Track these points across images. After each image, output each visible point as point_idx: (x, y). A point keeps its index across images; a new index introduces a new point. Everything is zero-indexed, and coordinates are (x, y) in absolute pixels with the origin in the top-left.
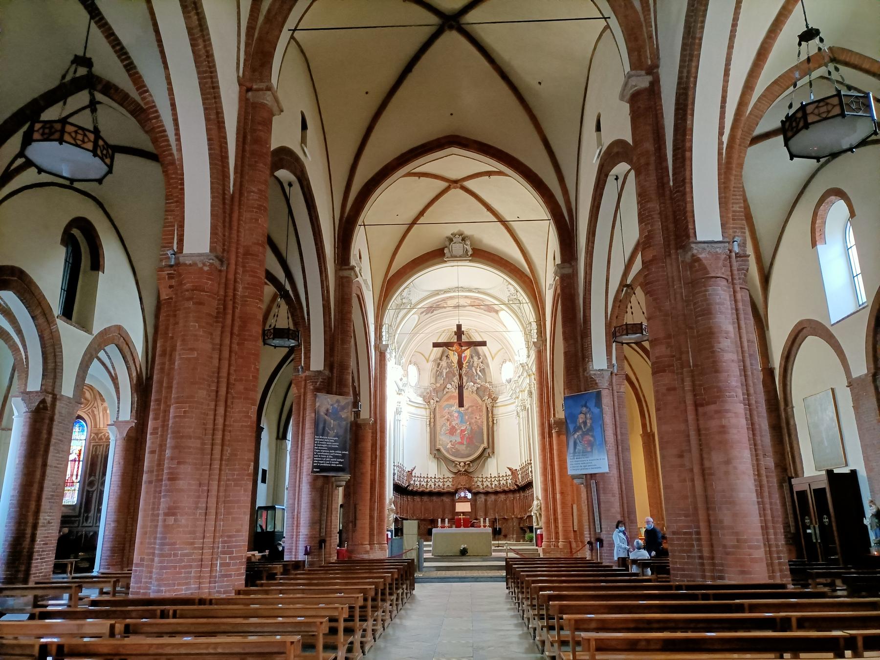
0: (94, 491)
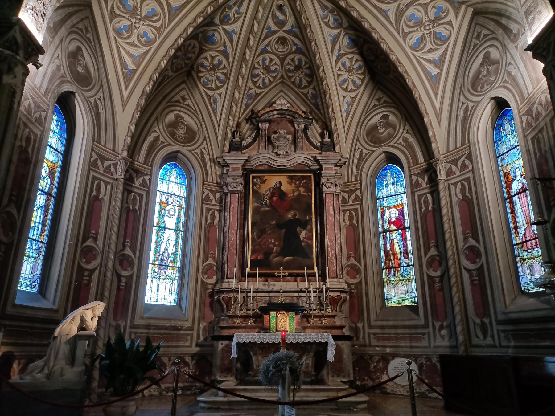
0: (92, 271)
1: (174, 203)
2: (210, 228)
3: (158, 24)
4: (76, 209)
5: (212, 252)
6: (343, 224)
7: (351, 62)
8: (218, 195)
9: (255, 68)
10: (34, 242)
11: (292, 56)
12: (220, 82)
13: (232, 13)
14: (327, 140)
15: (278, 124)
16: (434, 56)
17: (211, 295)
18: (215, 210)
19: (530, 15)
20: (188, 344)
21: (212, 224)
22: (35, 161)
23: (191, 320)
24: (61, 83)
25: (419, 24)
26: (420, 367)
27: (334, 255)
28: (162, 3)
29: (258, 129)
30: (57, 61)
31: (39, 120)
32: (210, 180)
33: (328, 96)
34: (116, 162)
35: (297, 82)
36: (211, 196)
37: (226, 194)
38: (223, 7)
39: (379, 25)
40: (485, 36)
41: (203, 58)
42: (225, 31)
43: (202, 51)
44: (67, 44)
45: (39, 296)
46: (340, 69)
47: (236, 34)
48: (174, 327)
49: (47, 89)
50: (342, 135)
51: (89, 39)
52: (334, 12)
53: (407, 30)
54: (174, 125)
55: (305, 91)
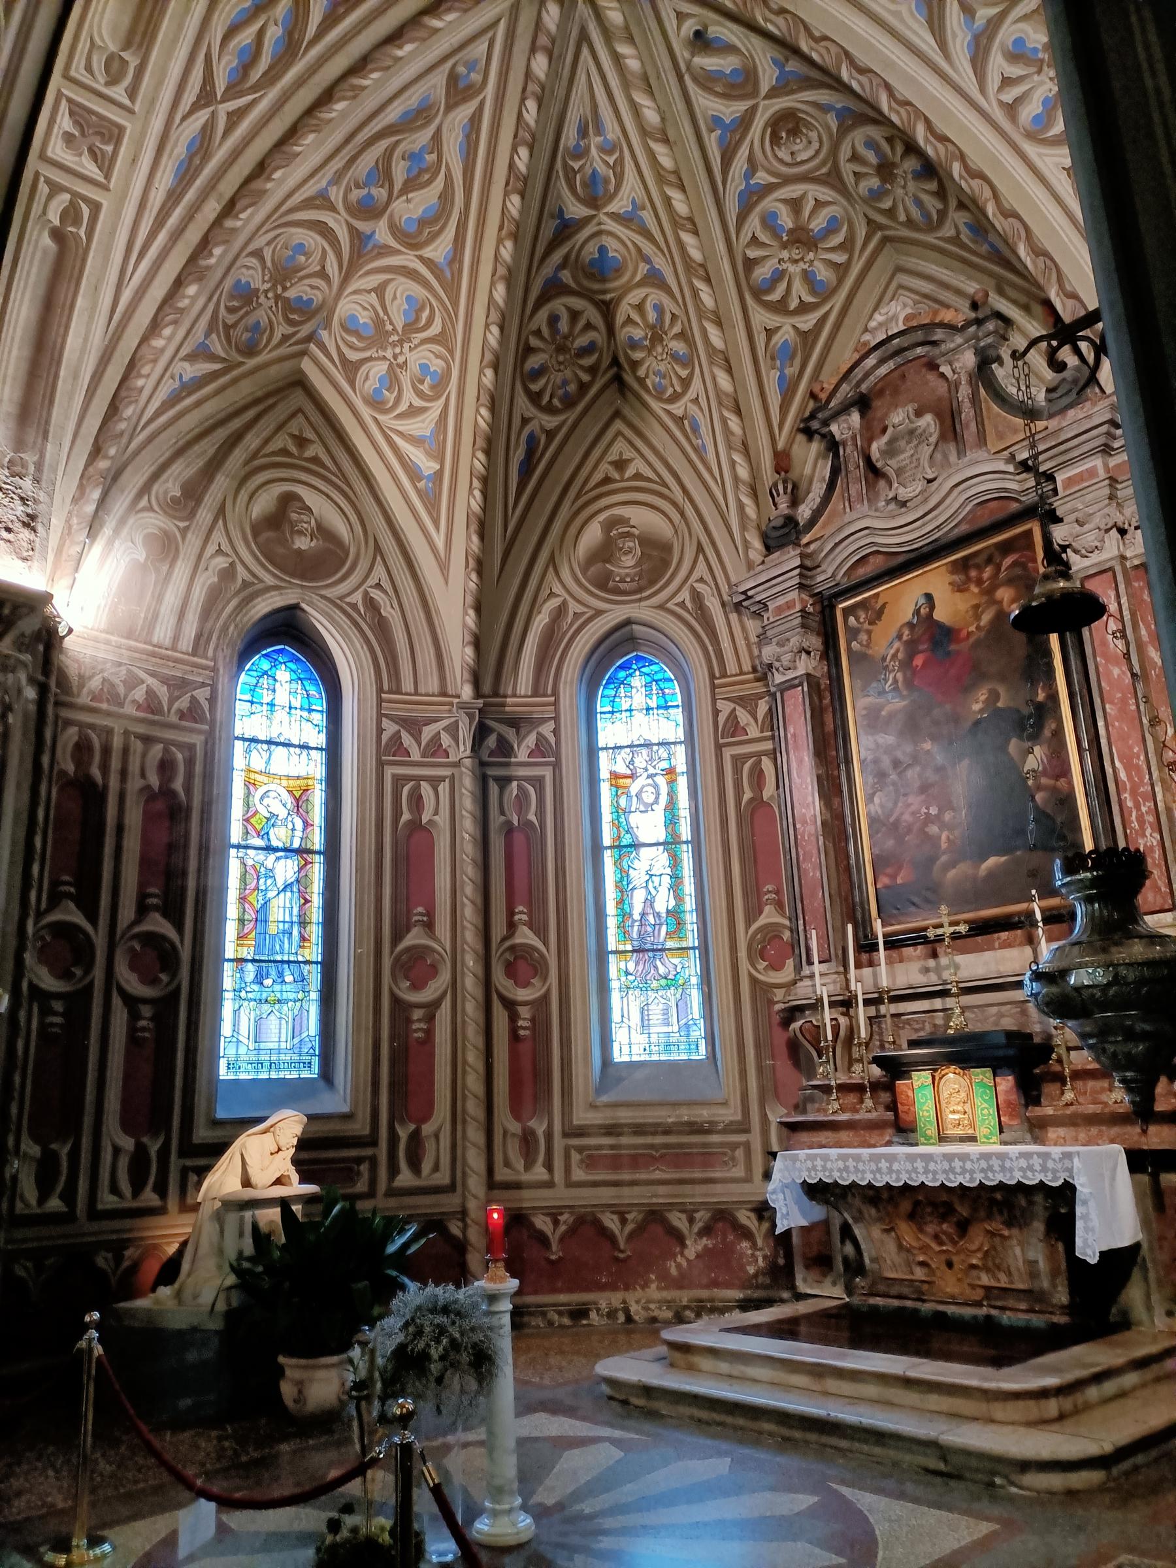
0: (432, 1007)
1: (649, 767)
2: (752, 814)
3: (435, 329)
5: (770, 887)
8: (763, 707)
9: (750, 264)
10: (286, 966)
11: (845, 152)
12: (684, 365)
18: (759, 755)
20: (739, 1172)
22: (203, 802)
23: (735, 1100)
27: (1150, 818)
29: (833, 445)
31: (192, 713)
32: (732, 667)
34: (453, 720)
35: (915, 213)
36: (743, 716)
38: (559, 165)
43: (607, 309)
44: (244, 505)
45: (322, 1084)
47: (643, 208)
48: (690, 1124)
49: (198, 637)
54: (605, 552)
55: (948, 231)
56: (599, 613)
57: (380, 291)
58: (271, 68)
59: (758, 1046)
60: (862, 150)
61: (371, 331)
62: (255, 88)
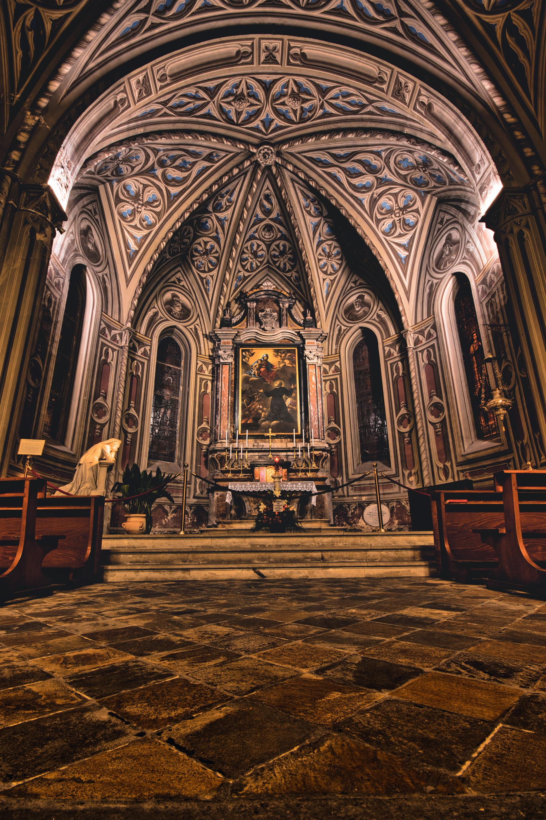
0: (103, 425)
3: (158, 210)
4: (88, 369)
6: (324, 392)
7: (330, 248)
8: (210, 367)
9: (244, 253)
11: (277, 243)
12: (212, 265)
13: (224, 202)
14: (309, 317)
15: (265, 303)
16: (404, 241)
17: (206, 455)
18: (208, 380)
19: (483, 191)
21: (205, 393)
24: (76, 256)
25: (390, 211)
26: (392, 511)
28: (162, 190)
30: (71, 235)
32: (203, 353)
33: (310, 278)
35: (282, 266)
37: (218, 366)
39: (356, 212)
40: (448, 220)
41: (197, 244)
42: (217, 218)
43: (196, 237)
46: (320, 254)
49: (64, 259)
50: (323, 313)
51: (97, 220)
52: (315, 201)
53: (379, 217)
54: (171, 303)
55: (289, 275)
56: (167, 320)
57: (145, 186)
58: (183, 112)
59: (196, 461)
60: (281, 246)
61: (133, 194)
62: (175, 113)
